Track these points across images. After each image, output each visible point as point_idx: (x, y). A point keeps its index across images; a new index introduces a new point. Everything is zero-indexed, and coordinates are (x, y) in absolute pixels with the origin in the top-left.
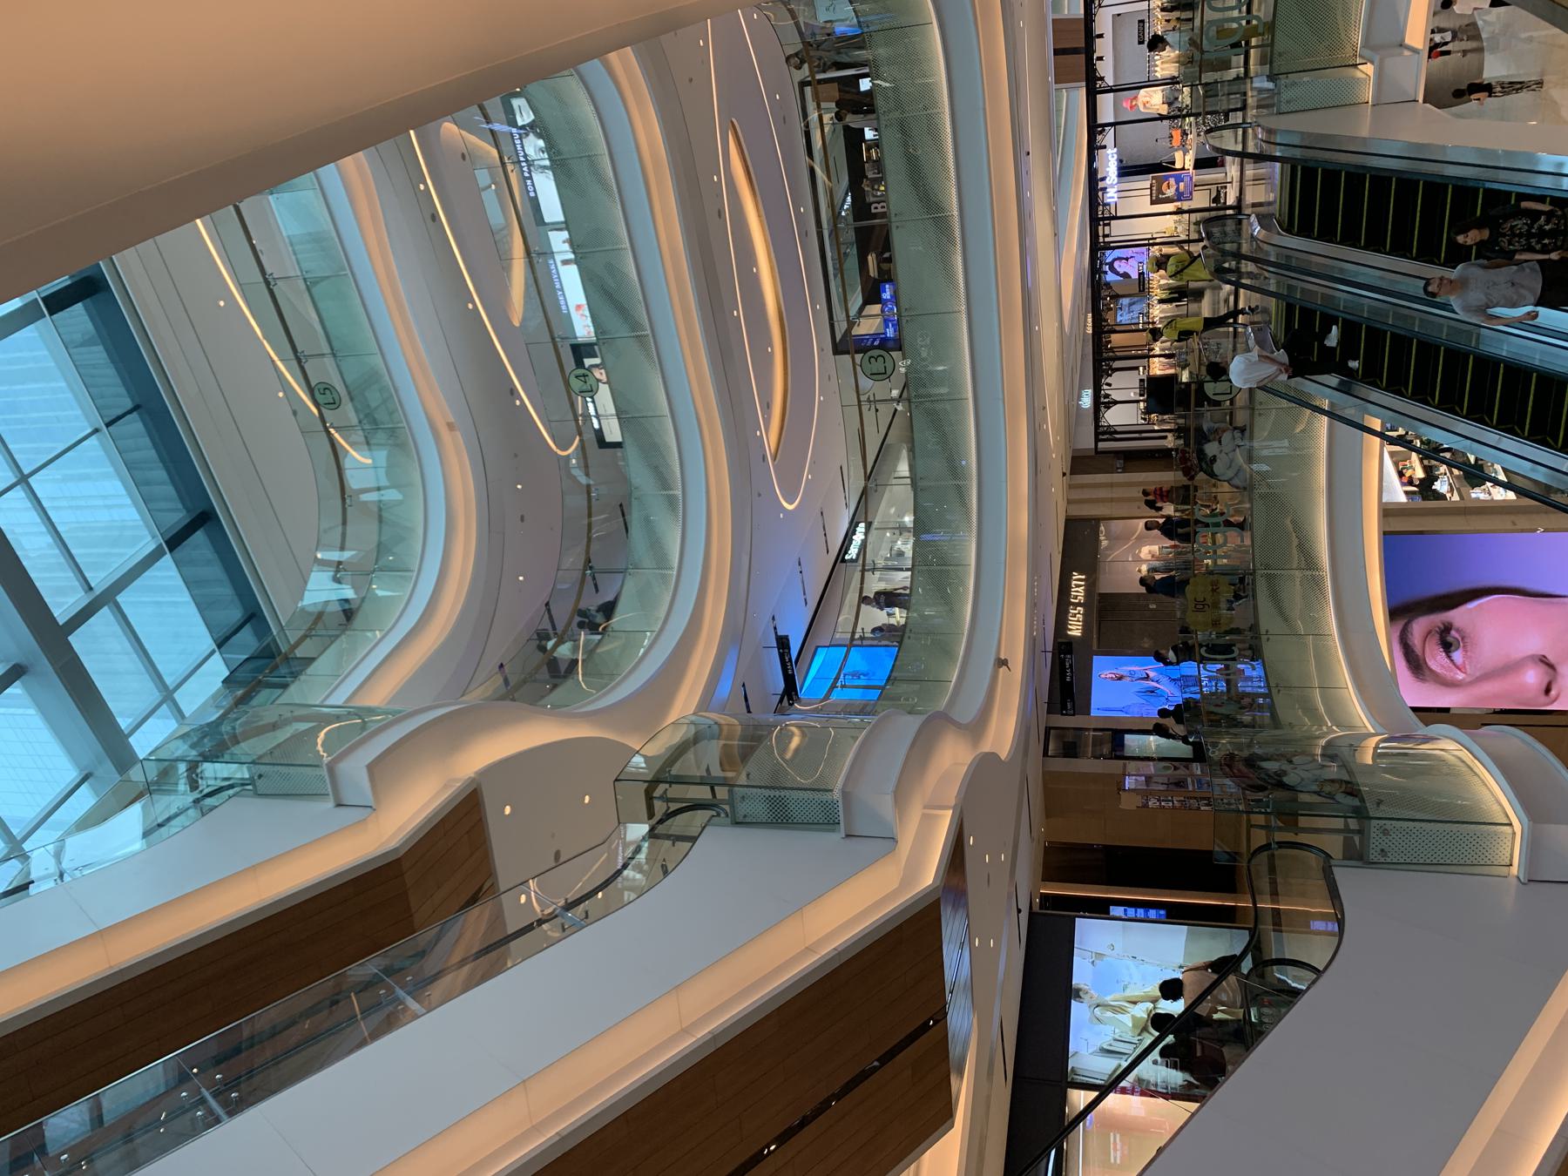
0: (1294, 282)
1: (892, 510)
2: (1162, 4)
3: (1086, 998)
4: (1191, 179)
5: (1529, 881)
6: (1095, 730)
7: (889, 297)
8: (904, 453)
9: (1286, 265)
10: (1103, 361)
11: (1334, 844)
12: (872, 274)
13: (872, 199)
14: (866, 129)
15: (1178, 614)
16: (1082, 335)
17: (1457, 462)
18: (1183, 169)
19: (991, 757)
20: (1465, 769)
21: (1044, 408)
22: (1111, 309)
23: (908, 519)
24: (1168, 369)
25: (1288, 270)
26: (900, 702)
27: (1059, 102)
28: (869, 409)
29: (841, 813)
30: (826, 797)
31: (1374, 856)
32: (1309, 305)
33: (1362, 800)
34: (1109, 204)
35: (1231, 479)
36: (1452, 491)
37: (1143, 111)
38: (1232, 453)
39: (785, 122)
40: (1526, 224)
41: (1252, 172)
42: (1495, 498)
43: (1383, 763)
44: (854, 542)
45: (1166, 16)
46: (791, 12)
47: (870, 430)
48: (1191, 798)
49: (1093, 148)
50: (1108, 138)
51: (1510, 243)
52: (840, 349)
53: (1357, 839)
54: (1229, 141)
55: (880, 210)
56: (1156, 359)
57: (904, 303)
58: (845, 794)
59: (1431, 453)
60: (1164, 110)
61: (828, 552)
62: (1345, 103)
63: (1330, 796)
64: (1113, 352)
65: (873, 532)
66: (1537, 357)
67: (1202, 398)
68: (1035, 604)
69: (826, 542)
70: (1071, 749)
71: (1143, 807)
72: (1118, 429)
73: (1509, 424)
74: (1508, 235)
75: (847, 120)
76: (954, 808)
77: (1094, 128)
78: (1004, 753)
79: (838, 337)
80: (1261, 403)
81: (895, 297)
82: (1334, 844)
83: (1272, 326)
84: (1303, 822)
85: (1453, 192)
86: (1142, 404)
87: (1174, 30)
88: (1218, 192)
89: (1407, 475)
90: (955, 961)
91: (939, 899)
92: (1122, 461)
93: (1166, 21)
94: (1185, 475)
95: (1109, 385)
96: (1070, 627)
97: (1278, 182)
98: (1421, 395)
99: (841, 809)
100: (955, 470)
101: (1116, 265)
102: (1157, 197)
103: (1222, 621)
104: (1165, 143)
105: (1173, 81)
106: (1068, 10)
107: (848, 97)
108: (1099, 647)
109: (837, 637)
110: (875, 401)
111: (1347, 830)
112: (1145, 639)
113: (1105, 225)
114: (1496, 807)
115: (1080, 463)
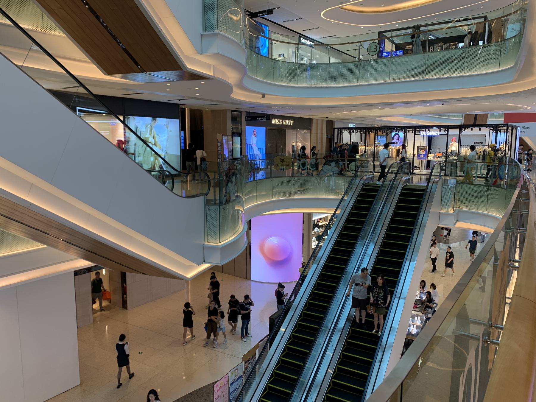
0: (386, 188)
1: (318, 56)
2: (486, 150)
3: (153, 122)
4: (424, 159)
5: (204, 247)
6: (241, 128)
7: (397, 53)
8: (339, 61)
9: (392, 187)
10: (365, 130)
11: (211, 196)
12: (407, 47)
13: (435, 47)
14: (463, 44)
15: (280, 154)
16: (374, 124)
17: (325, 233)
18: (428, 156)
19: (232, 91)
20: (235, 232)
21: (351, 111)
22: (383, 133)
23: (314, 62)
24: (361, 151)
25: (389, 192)
26: (249, 60)
27: (457, 116)
28: (357, 46)
29: (210, 33)
30: (215, 27)
31: (208, 207)
32: (377, 197)
33: (225, 204)
34: (420, 132)
35: (323, 170)
36: (315, 232)
37: (450, 144)
38: (331, 171)
39: (472, 10)
40: (381, 296)
41: (423, 177)
42: (313, 243)
43: (236, 213)
44: (307, 41)
45: (482, 151)
46: (517, 11)
47: (350, 47)
48: (221, 156)
49: (440, 127)
50: (443, 132)
51: (375, 291)
52: (380, 34)
53: (213, 203)
54: (436, 170)
55: (430, 50)
56: (364, 148)
57: (395, 59)
58: (217, 34)
59: (328, 227)
60: (449, 151)
61: (304, 30)
62: (442, 204)
63: (225, 196)
64: (368, 134)
65: (310, 49)
66: (334, 307)
67: (350, 162)
68: (283, 108)
69: (307, 30)
70: (234, 119)
71: (218, 141)
72: (342, 135)
73: (334, 251)
74: (378, 291)
75: (468, 36)
76: (214, 76)
77: (447, 128)
78: (232, 95)
79: (385, 34)
80: (347, 179)
81: (398, 56)
82: (211, 196)
83: (372, 183)
84: (217, 189)
85: (366, 375)
86: (349, 143)
87: (477, 154)
88: (418, 168)
89: (320, 221)
90: (160, 76)
91: (182, 70)
92: (330, 137)
93: (480, 151)
94: (325, 156)
95: (357, 133)
96: (275, 120)
97: (420, 185)
98: (344, 228)
99: (211, 33)
100: (332, 79)
101: (397, 136)
102: (420, 148)
103: (277, 167)
104: (438, 150)
105: (459, 153)
106: (490, 120)
107: (478, 35)
108: (269, 129)
109: (272, 34)
110: (360, 49)
111: (215, 200)
112: (270, 144)
113: (413, 131)
114: (224, 239)
115: (330, 123)
